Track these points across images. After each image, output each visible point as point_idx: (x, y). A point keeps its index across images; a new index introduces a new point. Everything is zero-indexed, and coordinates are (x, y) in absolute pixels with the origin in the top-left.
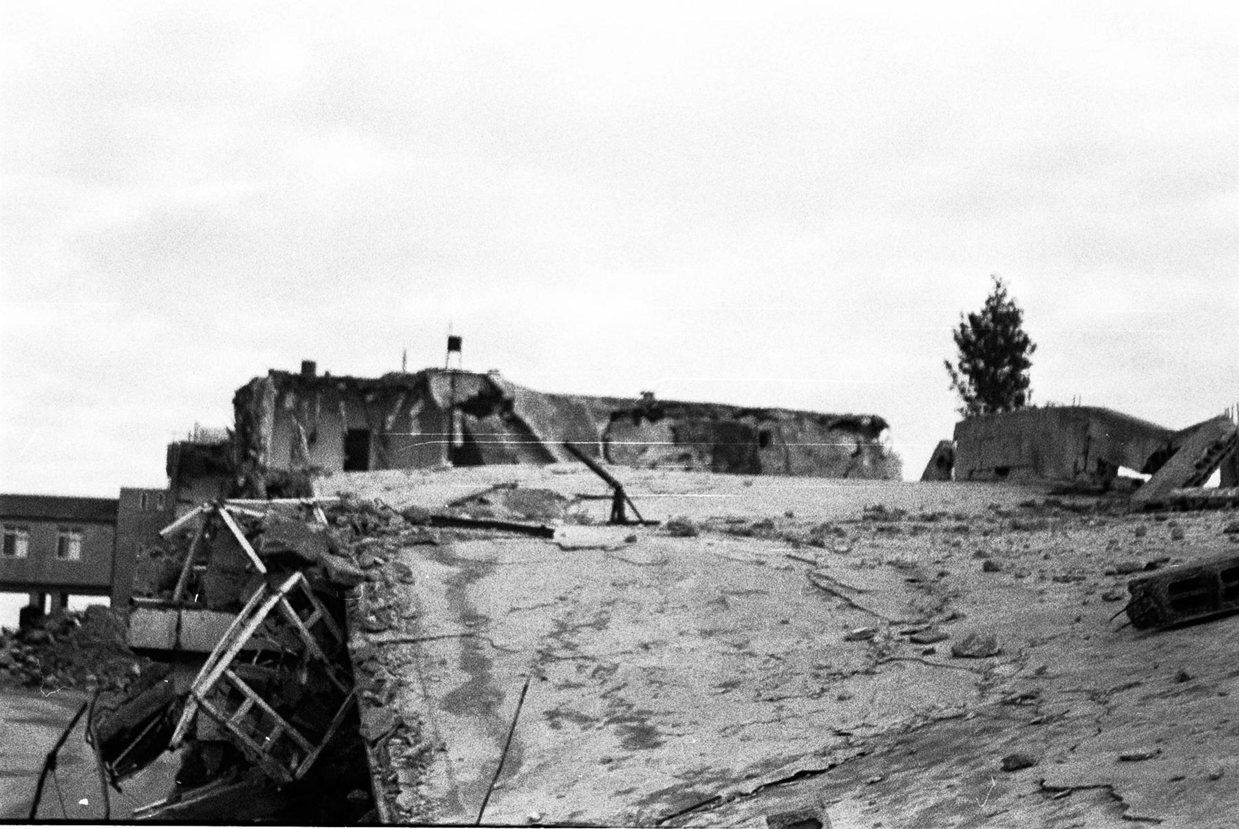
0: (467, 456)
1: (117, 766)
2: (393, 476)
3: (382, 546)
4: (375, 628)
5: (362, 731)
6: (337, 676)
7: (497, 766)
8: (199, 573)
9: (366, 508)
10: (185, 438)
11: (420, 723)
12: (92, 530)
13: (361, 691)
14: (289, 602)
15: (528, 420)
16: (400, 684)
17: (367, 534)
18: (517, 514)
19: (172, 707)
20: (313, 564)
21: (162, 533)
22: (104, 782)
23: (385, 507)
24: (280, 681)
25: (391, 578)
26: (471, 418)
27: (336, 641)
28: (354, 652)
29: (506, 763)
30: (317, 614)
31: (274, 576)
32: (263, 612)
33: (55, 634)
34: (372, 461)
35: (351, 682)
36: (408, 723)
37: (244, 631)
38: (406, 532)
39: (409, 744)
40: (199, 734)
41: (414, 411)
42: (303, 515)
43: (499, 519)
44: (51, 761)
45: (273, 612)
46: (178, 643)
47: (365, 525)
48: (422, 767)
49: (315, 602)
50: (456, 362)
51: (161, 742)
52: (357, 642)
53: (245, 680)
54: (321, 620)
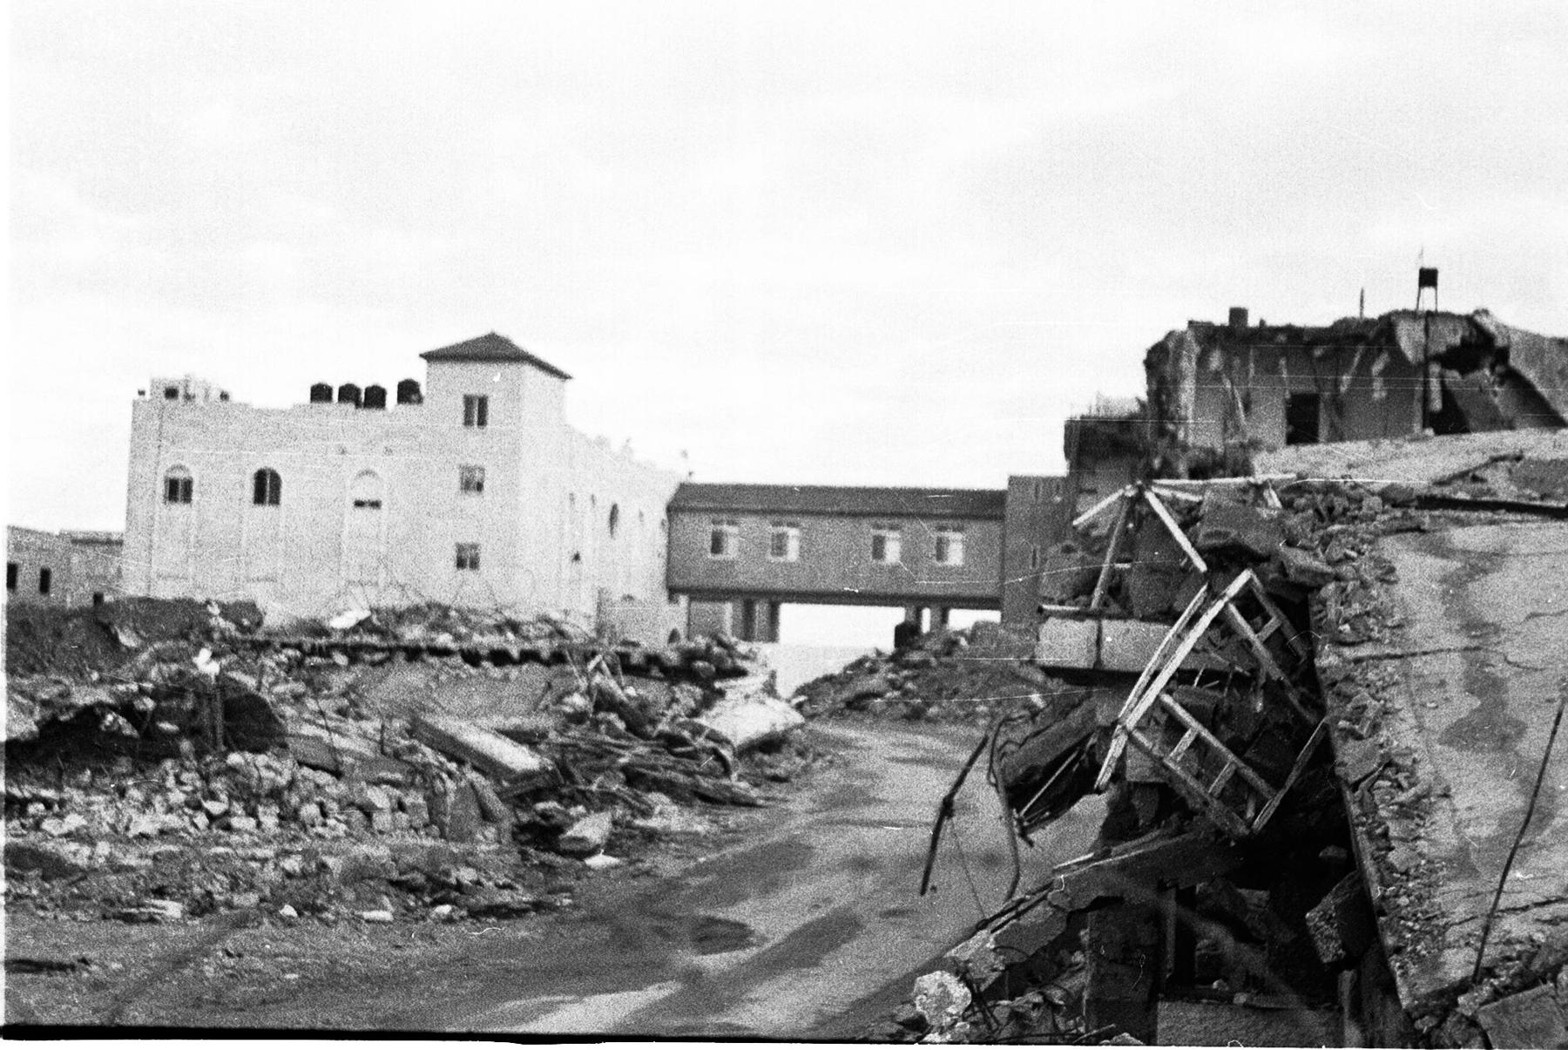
0: (1450, 421)
1: (1026, 814)
2: (1355, 449)
3: (1354, 535)
4: (1350, 640)
5: (1340, 771)
6: (1301, 702)
7: (1522, 818)
8: (1121, 573)
9: (1331, 488)
10: (1086, 412)
11: (1414, 761)
12: (975, 528)
13: (1337, 719)
14: (1238, 608)
15: (1531, 375)
16: (1386, 712)
17: (1333, 521)
18: (1528, 492)
19: (1092, 741)
20: (1267, 559)
21: (1075, 523)
22: (1012, 835)
23: (1355, 486)
24: (1230, 708)
25: (1367, 577)
26: (1453, 375)
27: (1298, 658)
28: (1324, 670)
29: (1535, 811)
30: (1273, 624)
31: (1220, 577)
32: (1205, 621)
33: (936, 654)
34: (1323, 431)
35: (1321, 710)
36: (1400, 761)
37: (1177, 646)
38: (1386, 517)
39: (1400, 787)
40: (1127, 776)
41: (1377, 367)
42: (1250, 497)
43: (1503, 497)
44: (947, 808)
45: (1216, 622)
46: (1098, 661)
47: (1331, 509)
48: (1422, 818)
49: (1269, 608)
50: (1429, 300)
51: (1083, 783)
52: (1328, 659)
53: (1184, 706)
54: (1278, 631)
